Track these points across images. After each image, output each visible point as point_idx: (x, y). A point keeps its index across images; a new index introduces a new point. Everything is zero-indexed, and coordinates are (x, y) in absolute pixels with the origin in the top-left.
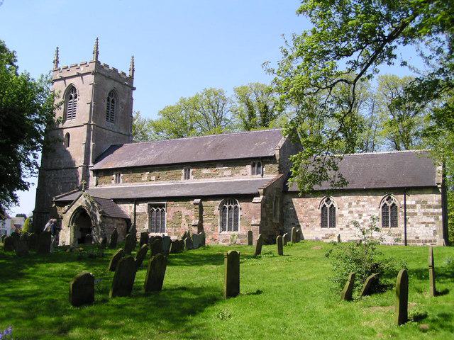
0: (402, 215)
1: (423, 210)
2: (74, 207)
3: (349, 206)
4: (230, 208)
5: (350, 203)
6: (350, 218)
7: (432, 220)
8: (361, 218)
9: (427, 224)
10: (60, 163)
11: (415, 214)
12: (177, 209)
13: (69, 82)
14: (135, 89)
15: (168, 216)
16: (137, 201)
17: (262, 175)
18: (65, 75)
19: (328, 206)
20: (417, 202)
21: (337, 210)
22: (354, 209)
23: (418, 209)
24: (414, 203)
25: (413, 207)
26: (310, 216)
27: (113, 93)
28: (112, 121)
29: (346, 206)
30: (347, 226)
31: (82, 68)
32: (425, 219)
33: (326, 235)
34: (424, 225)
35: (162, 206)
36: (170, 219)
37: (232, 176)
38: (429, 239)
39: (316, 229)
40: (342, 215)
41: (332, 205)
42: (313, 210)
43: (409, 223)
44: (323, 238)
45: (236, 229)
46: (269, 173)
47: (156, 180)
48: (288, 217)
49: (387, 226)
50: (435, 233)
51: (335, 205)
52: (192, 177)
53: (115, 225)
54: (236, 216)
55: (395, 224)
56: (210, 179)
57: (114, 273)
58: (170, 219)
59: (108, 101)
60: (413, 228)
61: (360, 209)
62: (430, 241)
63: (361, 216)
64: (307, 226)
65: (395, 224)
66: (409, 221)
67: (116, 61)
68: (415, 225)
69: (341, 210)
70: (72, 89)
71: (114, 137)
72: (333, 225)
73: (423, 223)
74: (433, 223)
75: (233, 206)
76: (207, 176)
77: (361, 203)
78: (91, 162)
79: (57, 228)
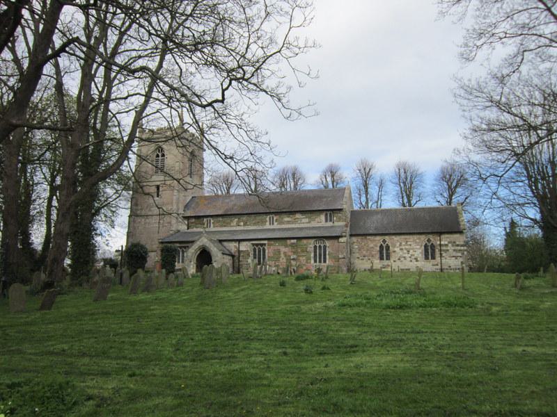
1: (453, 248)
3: (400, 245)
4: (320, 247)
5: (401, 243)
7: (460, 255)
9: (456, 257)
15: (269, 253)
16: (240, 241)
20: (449, 242)
22: (403, 247)
23: (450, 247)
24: (446, 243)
25: (446, 245)
29: (398, 244)
30: (399, 259)
32: (454, 254)
35: (262, 245)
37: (309, 222)
38: (458, 267)
45: (325, 262)
47: (244, 225)
50: (462, 263)
51: (390, 245)
52: (275, 223)
55: (433, 258)
61: (407, 247)
65: (433, 258)
66: (444, 255)
69: (394, 247)
77: (409, 243)
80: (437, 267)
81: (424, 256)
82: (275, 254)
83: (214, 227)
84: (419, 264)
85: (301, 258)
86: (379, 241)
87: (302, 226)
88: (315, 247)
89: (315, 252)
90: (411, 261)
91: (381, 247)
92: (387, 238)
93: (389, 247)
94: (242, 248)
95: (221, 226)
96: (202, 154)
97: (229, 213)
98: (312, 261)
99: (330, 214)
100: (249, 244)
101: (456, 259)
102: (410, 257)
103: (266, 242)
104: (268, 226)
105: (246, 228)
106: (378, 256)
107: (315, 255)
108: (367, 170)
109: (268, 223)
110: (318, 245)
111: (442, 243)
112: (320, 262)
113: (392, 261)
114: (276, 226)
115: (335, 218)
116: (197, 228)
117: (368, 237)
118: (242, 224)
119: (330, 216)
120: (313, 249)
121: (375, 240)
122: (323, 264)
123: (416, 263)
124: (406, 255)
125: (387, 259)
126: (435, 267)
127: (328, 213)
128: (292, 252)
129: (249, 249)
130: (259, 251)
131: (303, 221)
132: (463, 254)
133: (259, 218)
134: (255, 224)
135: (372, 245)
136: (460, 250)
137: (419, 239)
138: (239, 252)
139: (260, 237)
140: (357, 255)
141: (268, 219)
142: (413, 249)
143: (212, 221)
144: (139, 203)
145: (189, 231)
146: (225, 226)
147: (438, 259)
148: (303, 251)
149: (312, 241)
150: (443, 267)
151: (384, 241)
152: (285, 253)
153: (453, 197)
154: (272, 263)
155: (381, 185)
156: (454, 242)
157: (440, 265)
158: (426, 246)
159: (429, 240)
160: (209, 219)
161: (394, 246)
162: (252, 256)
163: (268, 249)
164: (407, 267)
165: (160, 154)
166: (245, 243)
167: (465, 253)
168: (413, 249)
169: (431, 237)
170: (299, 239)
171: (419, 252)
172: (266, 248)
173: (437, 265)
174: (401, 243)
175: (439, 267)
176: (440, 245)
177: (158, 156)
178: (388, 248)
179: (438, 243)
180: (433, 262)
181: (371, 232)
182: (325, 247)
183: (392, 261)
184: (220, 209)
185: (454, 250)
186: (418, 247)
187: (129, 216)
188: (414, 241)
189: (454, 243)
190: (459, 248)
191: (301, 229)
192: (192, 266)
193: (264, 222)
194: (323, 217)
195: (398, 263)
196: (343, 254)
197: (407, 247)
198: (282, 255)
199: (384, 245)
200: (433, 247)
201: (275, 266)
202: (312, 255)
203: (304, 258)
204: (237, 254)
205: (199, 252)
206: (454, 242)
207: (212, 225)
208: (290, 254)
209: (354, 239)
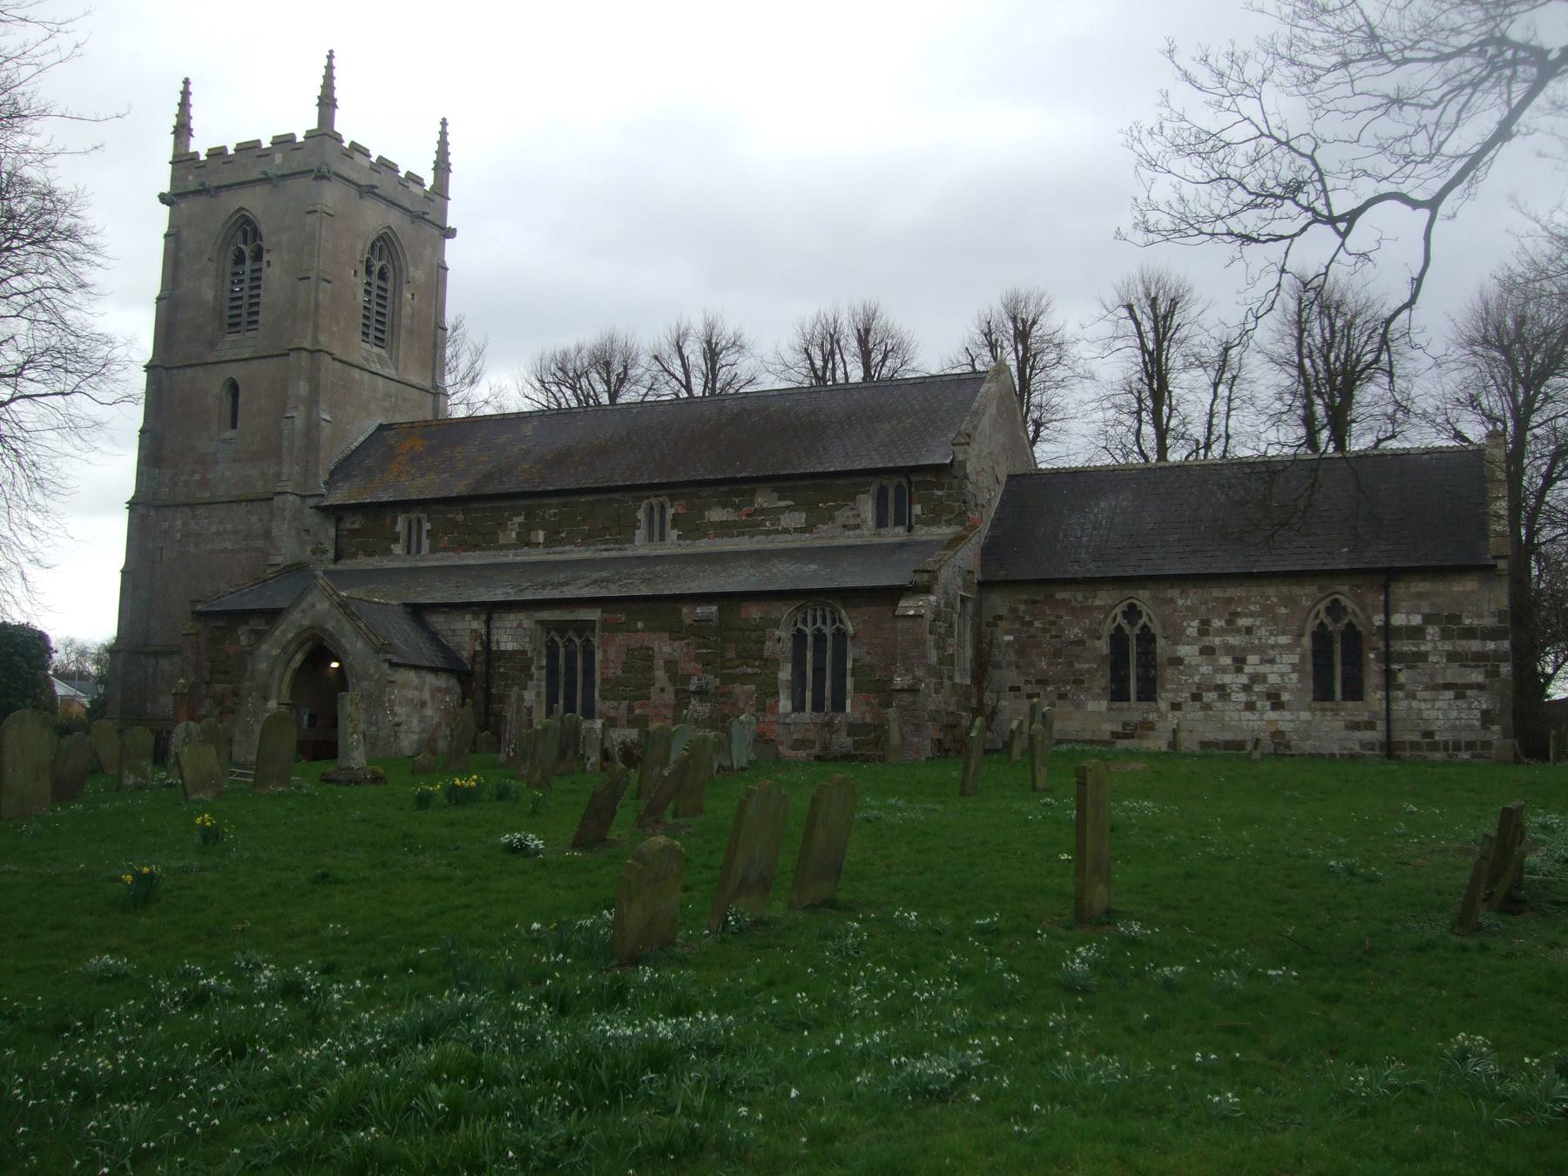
0: (1377, 660)
1: (1448, 646)
3: (1204, 631)
4: (819, 638)
5: (1205, 623)
6: (1203, 669)
7: (1477, 677)
9: (1460, 691)
14: (451, 233)
15: (605, 661)
16: (491, 610)
17: (910, 528)
19: (1132, 632)
20: (1428, 619)
21: (1161, 643)
23: (1433, 643)
24: (1416, 620)
25: (1416, 633)
26: (1071, 665)
27: (384, 244)
28: (380, 342)
29: (1192, 628)
30: (1196, 697)
32: (1453, 674)
33: (1125, 725)
34: (1450, 694)
35: (583, 627)
36: (615, 671)
37: (808, 528)
38: (1467, 736)
39: (1091, 706)
42: (1081, 642)
43: (1401, 687)
44: (1116, 735)
45: (839, 706)
46: (934, 522)
47: (550, 542)
48: (998, 666)
49: (1444, 741)
50: (1487, 718)
51: (1156, 628)
52: (673, 534)
53: (427, 688)
54: (840, 660)
55: (1354, 691)
58: (615, 671)
59: (369, 272)
60: (1415, 704)
61: (1233, 640)
62: (1470, 745)
63: (1239, 663)
64: (1063, 696)
66: (1402, 678)
67: (727, 329)
68: (1420, 695)
69: (1176, 643)
71: (388, 395)
73: (1447, 687)
74: (1480, 687)
76: (725, 529)
77: (1243, 622)
78: (829, 639)
80: (1368, 736)
81: (1310, 684)
83: (433, 550)
84: (1284, 720)
85: (737, 688)
86: (1107, 610)
87: (781, 542)
88: (799, 637)
89: (798, 663)
90: (1250, 706)
91: (1118, 639)
93: (1153, 639)
94: (506, 641)
95: (461, 547)
96: (439, 250)
97: (490, 490)
98: (785, 704)
99: (899, 488)
100: (526, 620)
101: (1460, 696)
102: (1246, 688)
103: (594, 615)
104: (640, 546)
105: (554, 556)
106: (1103, 679)
107: (799, 674)
108: (1162, 308)
109: (640, 534)
110: (808, 631)
111: (1398, 620)
113: (1163, 705)
114: (673, 543)
115: (917, 509)
117: (1061, 595)
118: (541, 536)
120: (788, 645)
123: (1272, 715)
124: (1227, 679)
126: (1358, 735)
127: (891, 485)
128: (698, 658)
129: (528, 647)
130: (571, 658)
131: (787, 520)
132: (1493, 674)
134: (588, 539)
135: (1074, 632)
136: (1480, 657)
137: (1290, 601)
139: (570, 592)
142: (1260, 650)
143: (427, 526)
145: (339, 566)
146: (476, 547)
147: (1375, 697)
149: (784, 611)
150: (1396, 738)
151: (1132, 613)
152: (670, 665)
153: (1536, 419)
155: (1223, 368)
156: (1455, 618)
157: (1381, 725)
158: (1322, 640)
159: (1335, 609)
160: (413, 516)
161: (1176, 637)
162: (539, 674)
166: (512, 620)
168: (1260, 650)
169: (1344, 593)
173: (1370, 725)
174: (1205, 623)
176: (1388, 632)
178: (1147, 638)
179: (1378, 620)
180: (1352, 708)
185: (1452, 657)
186: (1283, 640)
188: (1267, 611)
189: (1450, 624)
190: (1475, 645)
193: (623, 530)
195: (1192, 714)
196: (909, 670)
197: (1233, 640)
198: (660, 674)
199: (1132, 632)
200: (1353, 638)
202: (785, 674)
204: (480, 668)
205: (299, 657)
206: (1455, 618)
207: (426, 543)
208: (693, 666)
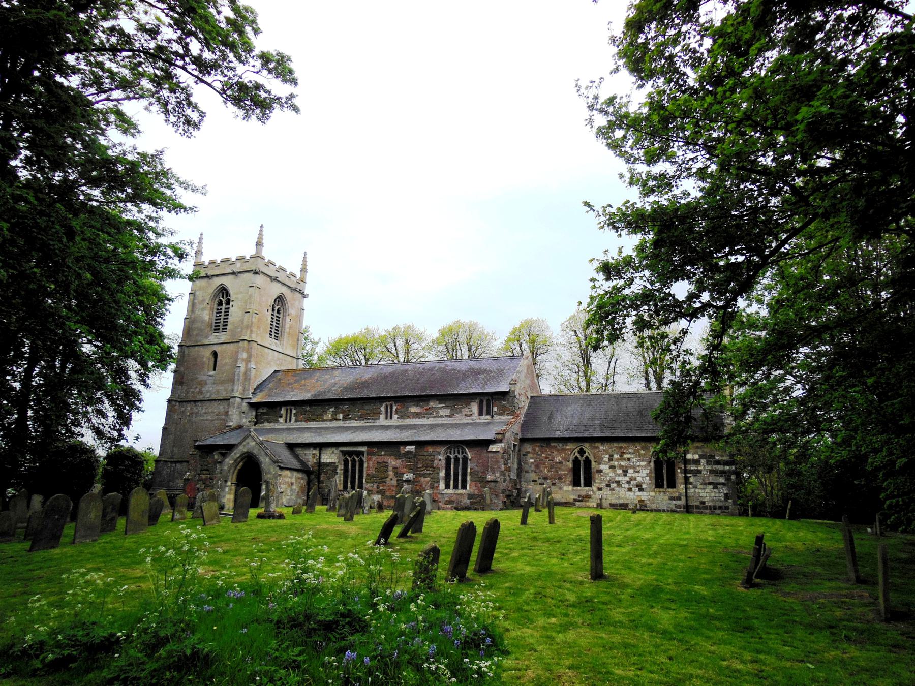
1: (710, 468)
2: (236, 454)
3: (611, 459)
5: (611, 456)
7: (722, 480)
8: (625, 475)
9: (716, 486)
10: (201, 392)
11: (700, 472)
12: (380, 459)
13: (217, 282)
15: (368, 467)
16: (321, 446)
17: (492, 417)
18: (210, 273)
19: (582, 459)
20: (701, 457)
21: (593, 464)
22: (616, 464)
23: (703, 466)
24: (696, 457)
25: (696, 462)
28: (276, 338)
29: (606, 459)
30: (608, 486)
31: (238, 264)
32: (712, 478)
33: (579, 496)
34: (711, 487)
38: (718, 504)
39: (565, 488)
40: (601, 471)
41: (587, 458)
42: (561, 463)
43: (691, 483)
45: (464, 487)
47: (344, 419)
48: (527, 472)
51: (591, 458)
52: (395, 417)
55: (672, 484)
56: (421, 420)
57: (468, 501)
58: (372, 471)
59: (273, 310)
60: (697, 490)
61: (623, 463)
63: (625, 472)
65: (672, 484)
66: (692, 480)
68: (699, 487)
69: (600, 464)
70: (223, 291)
72: (588, 483)
74: (723, 484)
75: (460, 456)
76: (417, 415)
77: (626, 456)
79: (759, 339)
80: (678, 502)
81: (654, 481)
82: (377, 470)
83: (296, 421)
84: (644, 496)
85: (422, 479)
87: (439, 421)
88: (448, 460)
90: (630, 490)
92: (586, 447)
93: (590, 462)
98: (442, 485)
99: (488, 401)
100: (336, 451)
101: (715, 487)
102: (628, 482)
103: (364, 449)
106: (570, 478)
109: (382, 416)
110: (452, 456)
112: (456, 487)
113: (595, 489)
115: (495, 409)
116: (270, 422)
118: (341, 416)
119: (488, 406)
121: (565, 450)
122: (460, 491)
124: (620, 478)
125: (585, 485)
126: (674, 502)
130: (354, 466)
131: (442, 412)
132: (728, 479)
133: (368, 407)
134: (361, 418)
135: (558, 459)
138: (320, 464)
140: (533, 476)
141: (383, 409)
142: (634, 467)
143: (294, 411)
144: (184, 380)
146: (314, 420)
148: (426, 467)
149: (442, 450)
151: (582, 452)
152: (395, 468)
154: (374, 487)
157: (683, 498)
163: (368, 460)
164: (621, 501)
165: (223, 300)
166: (330, 450)
167: (733, 477)
168: (634, 467)
170: (420, 444)
171: (644, 473)
172: (364, 459)
173: (679, 498)
175: (682, 502)
176: (686, 462)
177: (220, 303)
178: (588, 462)
181: (558, 434)
182: (465, 460)
183: (595, 489)
184: (308, 391)
185: (711, 472)
187: (169, 401)
188: (636, 452)
189: (710, 459)
190: (720, 468)
191: (432, 427)
192: (227, 489)
193: (375, 415)
194: (475, 407)
195: (606, 492)
196: (493, 473)
197: (623, 463)
199: (582, 459)
201: (378, 493)
202: (442, 474)
203: (428, 479)
207: (293, 418)
209: (528, 447)
